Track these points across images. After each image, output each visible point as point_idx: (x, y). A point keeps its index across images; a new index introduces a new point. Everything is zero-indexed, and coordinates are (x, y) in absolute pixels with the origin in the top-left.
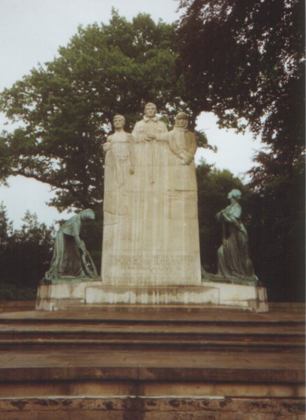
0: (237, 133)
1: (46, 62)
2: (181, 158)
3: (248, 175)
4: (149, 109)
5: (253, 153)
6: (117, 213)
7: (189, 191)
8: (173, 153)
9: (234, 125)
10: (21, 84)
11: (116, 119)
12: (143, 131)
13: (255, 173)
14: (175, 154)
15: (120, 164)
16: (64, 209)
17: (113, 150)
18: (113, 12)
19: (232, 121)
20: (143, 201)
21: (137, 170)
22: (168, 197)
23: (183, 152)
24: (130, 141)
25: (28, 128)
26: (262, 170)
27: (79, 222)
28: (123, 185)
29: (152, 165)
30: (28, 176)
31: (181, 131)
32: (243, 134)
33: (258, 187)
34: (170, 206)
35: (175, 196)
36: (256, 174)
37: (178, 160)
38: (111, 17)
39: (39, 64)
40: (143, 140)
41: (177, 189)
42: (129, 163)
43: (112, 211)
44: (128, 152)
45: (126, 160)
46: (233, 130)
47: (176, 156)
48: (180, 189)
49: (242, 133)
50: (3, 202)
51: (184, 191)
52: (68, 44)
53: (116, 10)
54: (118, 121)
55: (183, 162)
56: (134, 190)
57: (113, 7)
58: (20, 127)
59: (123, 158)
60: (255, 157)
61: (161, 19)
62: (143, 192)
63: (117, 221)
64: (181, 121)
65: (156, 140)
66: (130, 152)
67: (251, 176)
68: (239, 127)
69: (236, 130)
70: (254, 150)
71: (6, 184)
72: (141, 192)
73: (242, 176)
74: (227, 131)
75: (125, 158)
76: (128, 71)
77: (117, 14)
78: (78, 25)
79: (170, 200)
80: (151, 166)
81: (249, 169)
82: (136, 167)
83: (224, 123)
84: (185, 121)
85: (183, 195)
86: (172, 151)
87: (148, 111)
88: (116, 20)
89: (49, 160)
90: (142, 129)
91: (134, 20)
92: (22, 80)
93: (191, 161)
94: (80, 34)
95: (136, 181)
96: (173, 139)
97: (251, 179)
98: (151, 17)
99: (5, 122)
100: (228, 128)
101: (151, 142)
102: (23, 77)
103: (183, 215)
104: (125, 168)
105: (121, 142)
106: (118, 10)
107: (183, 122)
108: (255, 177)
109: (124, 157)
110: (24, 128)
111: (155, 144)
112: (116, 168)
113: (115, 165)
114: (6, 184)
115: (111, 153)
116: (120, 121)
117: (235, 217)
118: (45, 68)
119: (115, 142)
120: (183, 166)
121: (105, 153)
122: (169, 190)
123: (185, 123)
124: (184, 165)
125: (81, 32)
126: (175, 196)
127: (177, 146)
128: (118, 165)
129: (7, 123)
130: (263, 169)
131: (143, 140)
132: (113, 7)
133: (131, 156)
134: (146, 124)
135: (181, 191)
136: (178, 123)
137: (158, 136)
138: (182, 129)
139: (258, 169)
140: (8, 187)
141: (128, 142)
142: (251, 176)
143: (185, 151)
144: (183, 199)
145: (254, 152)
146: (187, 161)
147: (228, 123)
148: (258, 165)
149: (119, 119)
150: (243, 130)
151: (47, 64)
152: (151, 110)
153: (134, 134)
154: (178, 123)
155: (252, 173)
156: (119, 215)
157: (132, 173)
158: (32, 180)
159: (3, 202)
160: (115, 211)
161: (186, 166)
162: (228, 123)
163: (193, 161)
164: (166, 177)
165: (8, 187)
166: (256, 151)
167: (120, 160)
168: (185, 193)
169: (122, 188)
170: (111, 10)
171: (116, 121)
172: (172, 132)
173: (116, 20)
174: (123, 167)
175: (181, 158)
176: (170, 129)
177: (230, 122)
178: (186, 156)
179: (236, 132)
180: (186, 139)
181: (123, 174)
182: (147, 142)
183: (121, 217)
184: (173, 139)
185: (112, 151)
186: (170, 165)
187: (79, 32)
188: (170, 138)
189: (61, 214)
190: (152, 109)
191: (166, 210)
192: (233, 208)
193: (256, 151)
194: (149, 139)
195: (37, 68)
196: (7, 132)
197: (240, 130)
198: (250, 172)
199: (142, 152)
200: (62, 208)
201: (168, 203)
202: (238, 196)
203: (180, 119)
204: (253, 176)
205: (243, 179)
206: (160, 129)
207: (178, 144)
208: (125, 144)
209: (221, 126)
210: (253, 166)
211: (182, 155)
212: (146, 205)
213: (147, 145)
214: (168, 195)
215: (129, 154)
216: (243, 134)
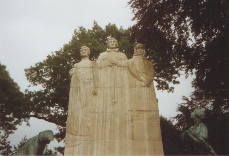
0: (169, 92)
1: (56, 51)
2: (142, 81)
3: (175, 120)
4: (111, 42)
5: (177, 106)
6: (78, 135)
7: (150, 111)
8: (133, 77)
9: (167, 88)
10: (41, 64)
11: (82, 49)
12: (106, 58)
13: (179, 118)
14: (136, 77)
15: (84, 86)
16: (61, 140)
17: (78, 75)
18: (95, 23)
19: (165, 85)
20: (106, 121)
21: (99, 91)
22: (130, 118)
23: (142, 75)
24: (94, 66)
25: (45, 90)
26: (183, 116)
27: (36, 144)
28: (86, 105)
29: (114, 87)
30: (40, 118)
31: (140, 58)
32: (173, 93)
33: (182, 126)
34: (133, 126)
35: (137, 116)
36: (180, 119)
37: (138, 82)
38: (93, 26)
39: (52, 53)
40: (106, 65)
41: (138, 109)
42: (92, 85)
43: (74, 133)
44: (92, 75)
45: (90, 82)
46: (166, 91)
47: (136, 79)
48: (141, 109)
49: (171, 92)
50: (26, 136)
51: (146, 111)
52: (70, 42)
53: (96, 22)
54: (83, 50)
55: (143, 84)
56: (97, 111)
57: (94, 21)
58: (40, 90)
59: (87, 81)
60: (177, 109)
61: (121, 27)
62: (106, 112)
63: (78, 142)
64: (139, 50)
65: (117, 65)
66: (94, 76)
67: (177, 120)
68: (170, 88)
69: (168, 90)
70: (178, 104)
71: (28, 124)
72: (103, 112)
73: (172, 120)
74: (162, 91)
75: (89, 81)
76: (102, 49)
77: (96, 24)
78: (74, 30)
79: (132, 120)
80: (113, 88)
81: (176, 116)
82: (99, 89)
83: (161, 86)
84: (142, 50)
85: (145, 115)
86: (132, 74)
87: (110, 44)
88: (96, 27)
89: (58, 110)
90: (104, 57)
91: (107, 27)
92: (42, 62)
93: (151, 84)
94: (76, 35)
95: (99, 102)
96: (133, 64)
97: (177, 121)
98: (116, 26)
99: (29, 85)
100: (163, 89)
101: (113, 67)
102: (43, 61)
103: (146, 135)
104: (88, 90)
105: (86, 67)
106: (97, 22)
107: (141, 51)
108: (179, 120)
109: (88, 79)
110: (43, 91)
111: (117, 70)
112: (80, 89)
113: (79, 87)
114: (28, 124)
115: (76, 76)
116: (85, 50)
117: (203, 137)
118: (55, 54)
119: (80, 68)
120: (143, 88)
121: (71, 76)
122: (131, 111)
123: (143, 52)
124: (144, 87)
125: (76, 33)
126: (137, 116)
127: (136, 70)
128: (81, 86)
129: (30, 86)
130: (184, 115)
131: (106, 65)
132: (94, 21)
133: (95, 78)
134: (108, 54)
135: (143, 111)
136: (137, 52)
137: (119, 62)
138: (141, 57)
139: (181, 115)
140: (30, 126)
141: (92, 67)
142: (177, 120)
143: (144, 75)
144: (145, 120)
145: (178, 105)
146: (146, 83)
147: (163, 86)
148: (180, 113)
149: (85, 49)
150: (172, 90)
151: (56, 52)
152: (112, 43)
153: (98, 61)
154: (137, 52)
155: (177, 118)
156: (81, 136)
157: (95, 94)
158: (43, 121)
159: (26, 136)
160: (77, 132)
161: (146, 88)
162: (163, 86)
163: (152, 83)
164: (127, 99)
165: (30, 126)
166: (179, 105)
167: (84, 83)
168: (147, 113)
169: (84, 108)
170: (93, 22)
171: (82, 50)
172: (131, 60)
173: (96, 27)
174: (87, 89)
175: (142, 81)
176: (129, 57)
177: (164, 86)
178: (146, 79)
179: (168, 91)
180: (145, 64)
181: (87, 96)
182: (109, 67)
183: (83, 138)
184: (133, 64)
185: (77, 75)
186: (131, 86)
187: (75, 33)
188: (131, 64)
189: (60, 143)
190: (114, 42)
191: (128, 130)
192: (199, 128)
193: (179, 105)
194: (111, 65)
195: (51, 55)
196: (28, 90)
197: (171, 90)
198: (176, 117)
199: (104, 76)
200: (60, 139)
201: (130, 124)
202: (202, 116)
203: (139, 48)
204: (178, 120)
205: (173, 121)
206: (121, 57)
207: (138, 68)
208: (90, 69)
209: (159, 88)
210: (178, 114)
211: (142, 78)
212: (108, 126)
213: (109, 69)
214: (130, 115)
215: (92, 77)
216: (173, 93)
